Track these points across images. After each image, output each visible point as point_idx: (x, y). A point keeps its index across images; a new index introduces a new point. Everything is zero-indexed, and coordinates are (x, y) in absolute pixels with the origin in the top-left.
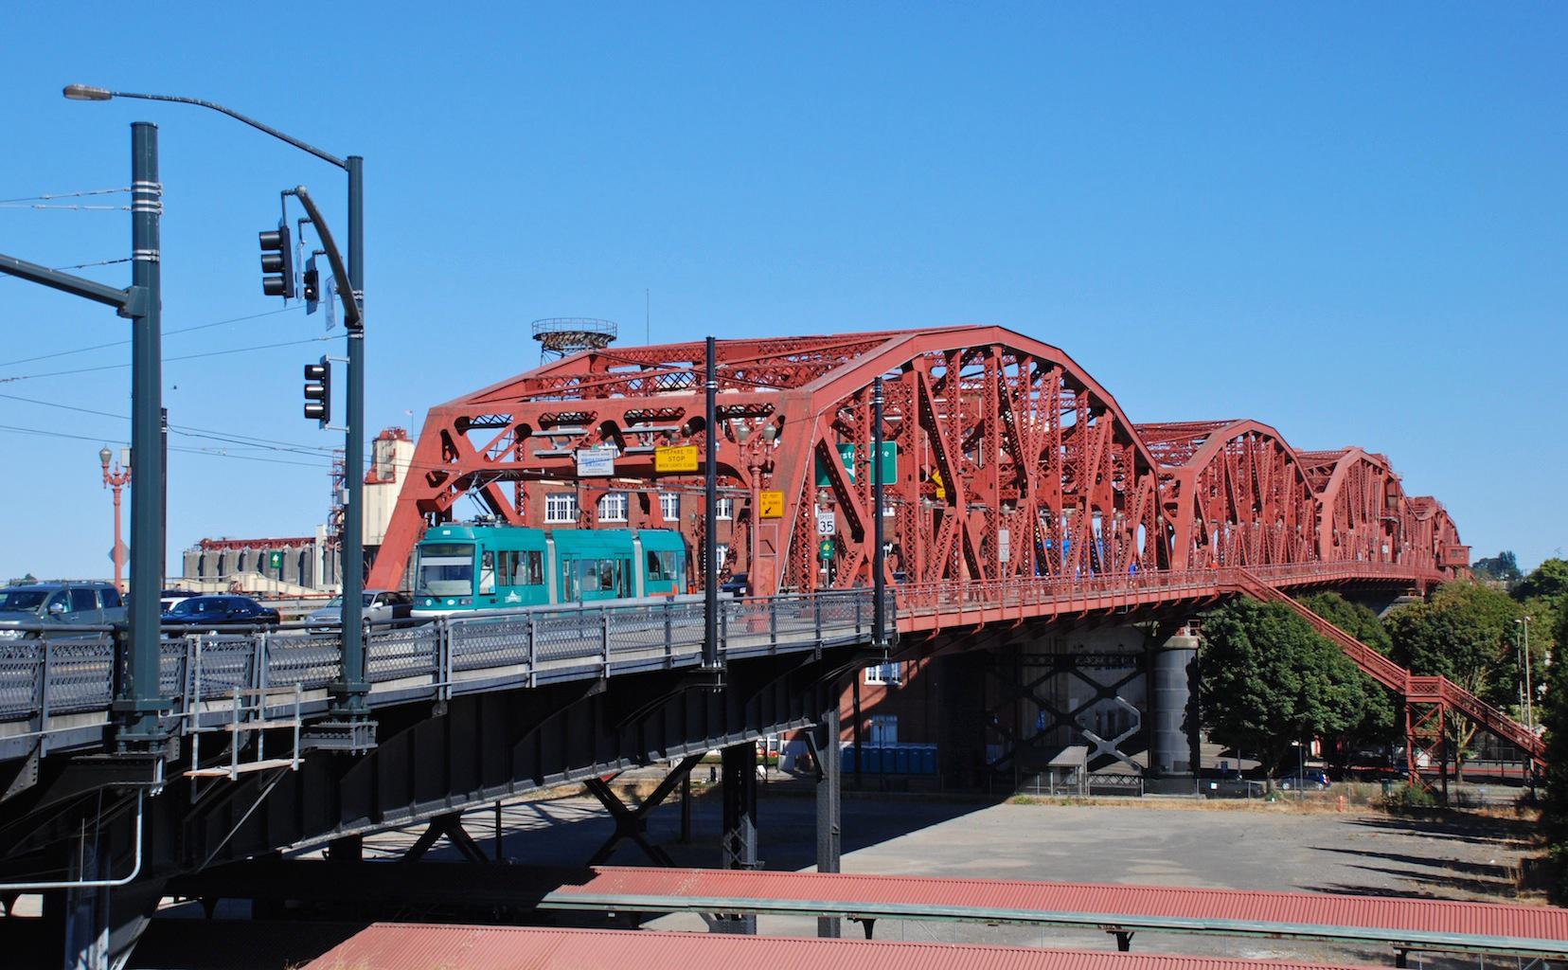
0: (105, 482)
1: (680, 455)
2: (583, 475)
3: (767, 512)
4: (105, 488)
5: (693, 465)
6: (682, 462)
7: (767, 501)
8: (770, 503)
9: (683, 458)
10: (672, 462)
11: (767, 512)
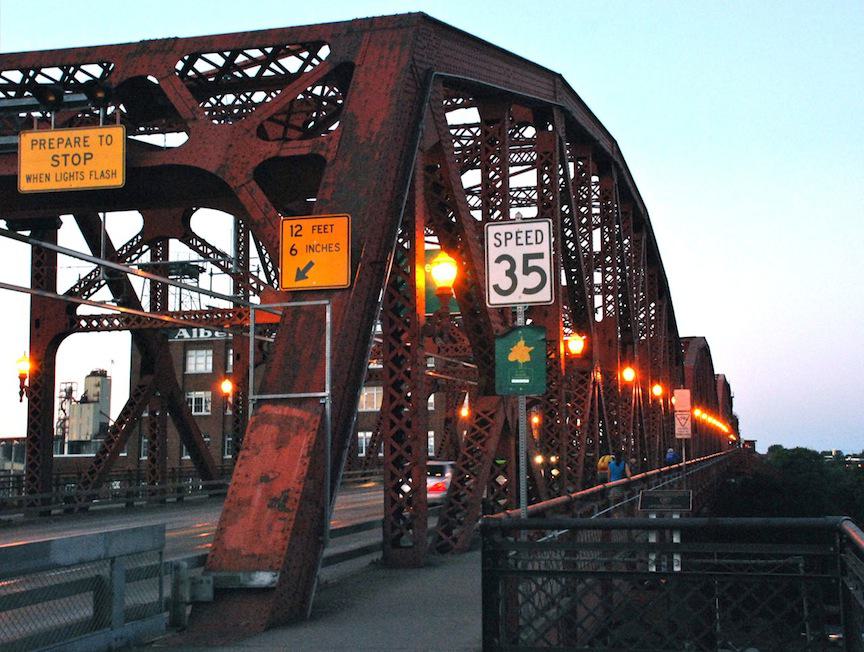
1: (81, 151)
3: (301, 275)
4: (21, 401)
5: (114, 174)
6: (86, 168)
7: (300, 244)
8: (310, 248)
9: (88, 157)
10: (62, 168)
11: (301, 275)
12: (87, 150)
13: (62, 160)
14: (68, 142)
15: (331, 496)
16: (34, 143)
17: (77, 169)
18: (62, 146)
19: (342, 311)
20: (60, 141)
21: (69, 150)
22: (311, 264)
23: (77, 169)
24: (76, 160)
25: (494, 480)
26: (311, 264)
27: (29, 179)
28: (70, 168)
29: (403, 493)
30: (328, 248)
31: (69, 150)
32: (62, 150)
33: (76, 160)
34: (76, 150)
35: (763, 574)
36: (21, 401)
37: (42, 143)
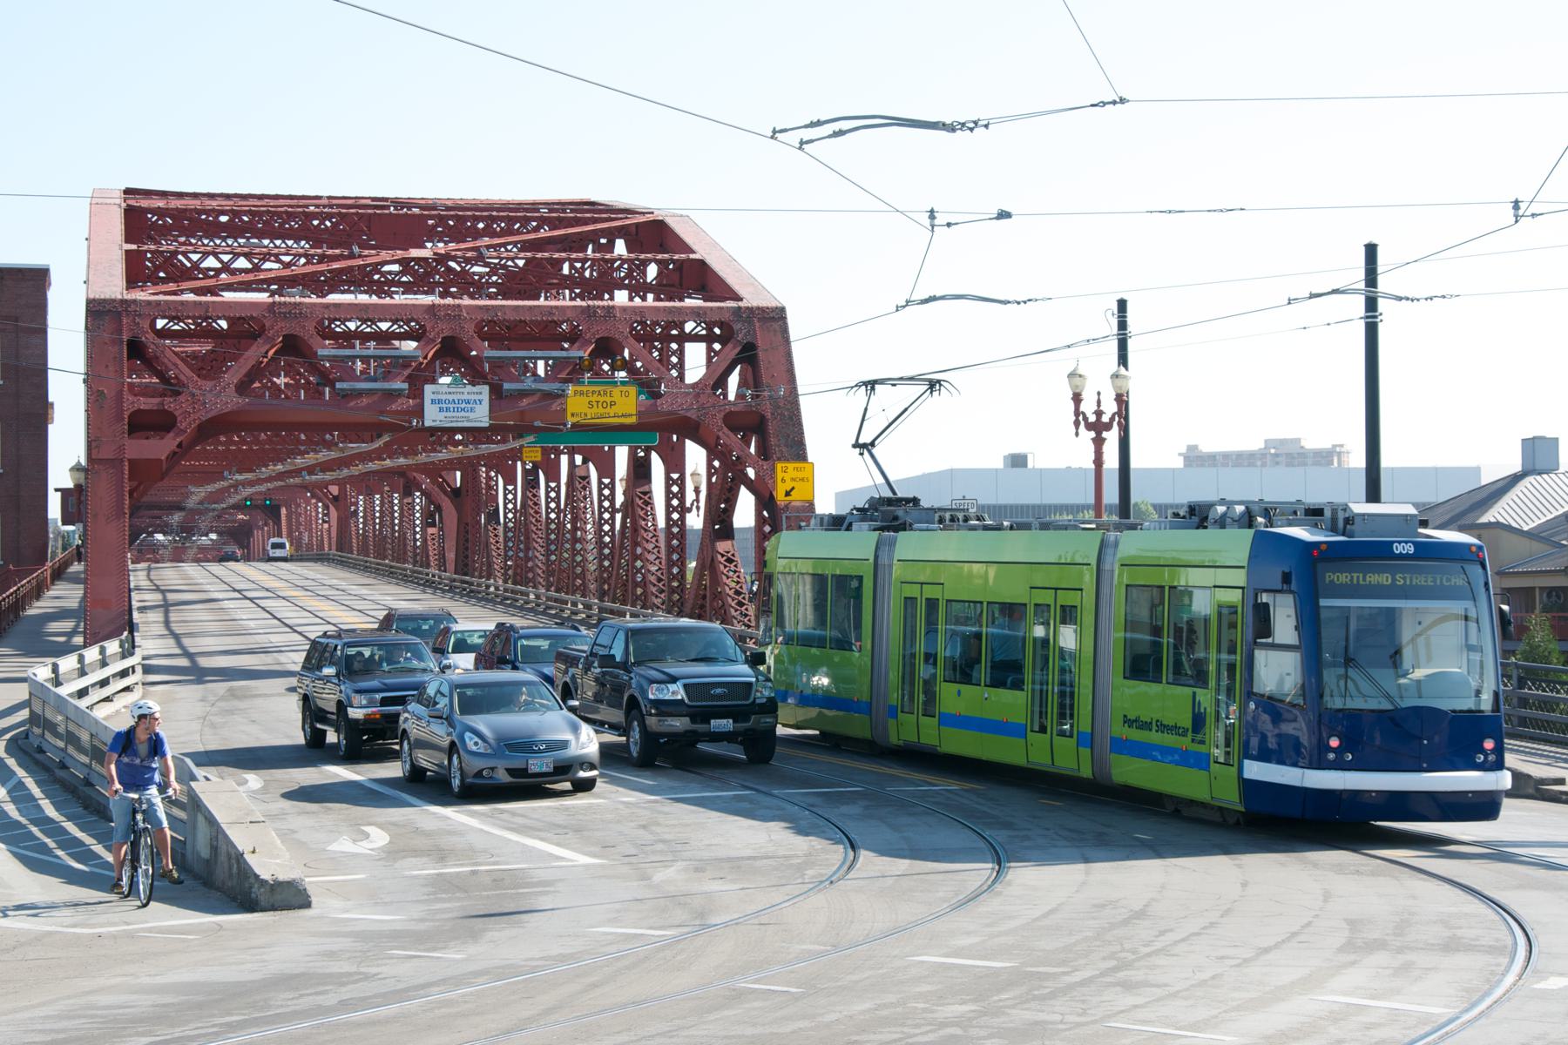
0: (1077, 424)
1: (608, 399)
2: (437, 424)
3: (788, 494)
4: (1077, 434)
7: (787, 477)
8: (793, 480)
9: (613, 404)
10: (595, 410)
11: (788, 494)
12: (613, 399)
13: (595, 404)
14: (599, 394)
15: (644, 213)
16: (576, 393)
17: (606, 410)
18: (595, 395)
19: (494, 1033)
20: (593, 392)
21: (601, 399)
22: (793, 488)
23: (606, 410)
24: (605, 405)
25: (680, 489)
26: (793, 488)
27: (573, 415)
28: (601, 410)
29: (608, 364)
30: (802, 480)
31: (601, 399)
32: (595, 398)
33: (605, 405)
34: (605, 399)
35: (494, 448)
36: (1077, 434)
37: (582, 393)
